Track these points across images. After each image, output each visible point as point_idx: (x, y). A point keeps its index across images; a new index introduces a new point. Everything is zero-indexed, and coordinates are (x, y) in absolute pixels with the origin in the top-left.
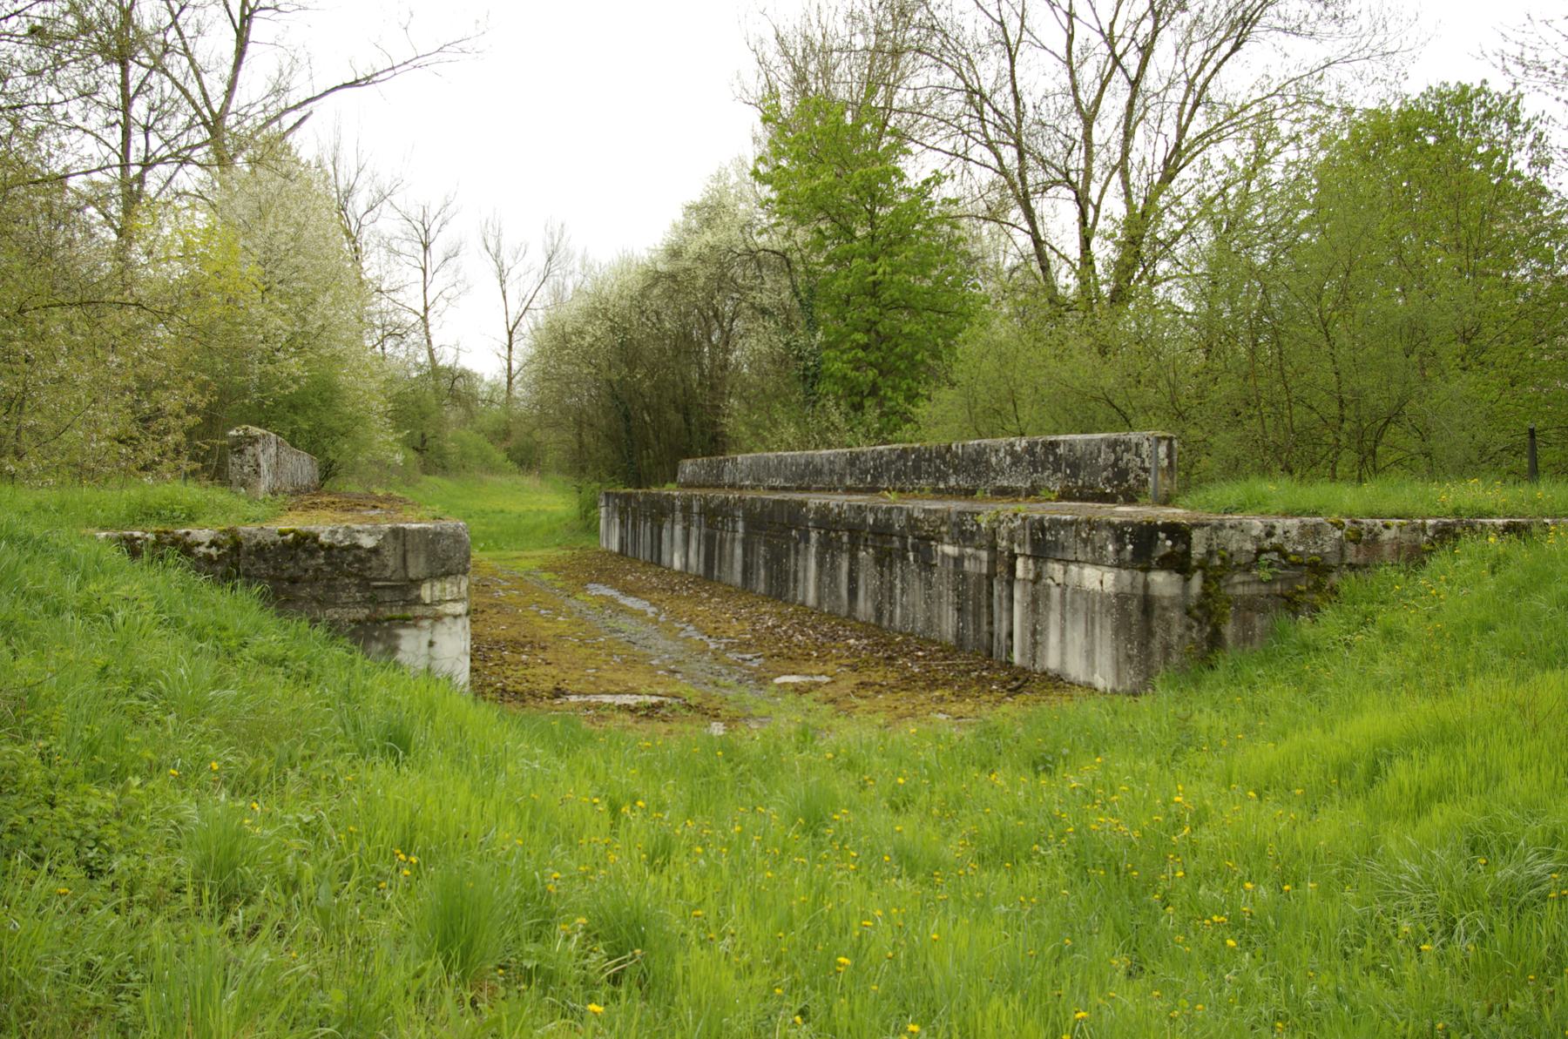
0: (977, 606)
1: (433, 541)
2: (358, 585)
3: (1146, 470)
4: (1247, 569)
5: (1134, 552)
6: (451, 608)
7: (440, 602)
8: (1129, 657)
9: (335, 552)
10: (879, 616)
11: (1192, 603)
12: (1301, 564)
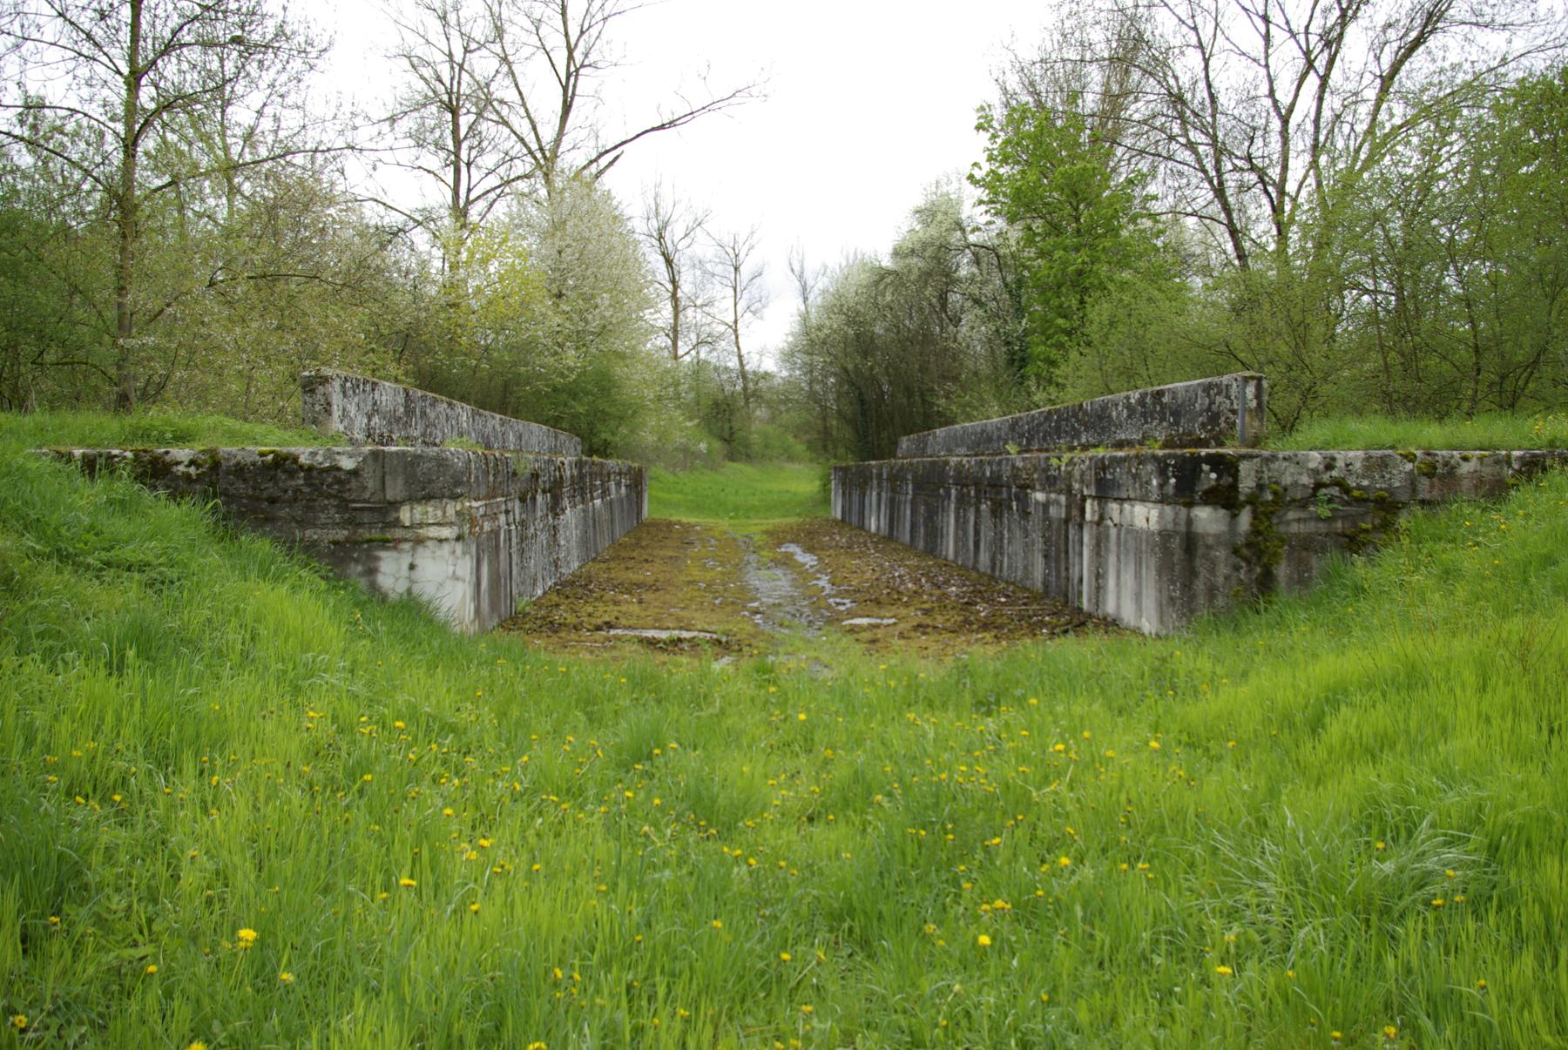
0: (1058, 555)
1: (412, 464)
2: (337, 506)
3: (1234, 412)
4: (1303, 504)
5: (1177, 486)
6: (433, 532)
7: (421, 525)
8: (1172, 599)
9: (315, 473)
10: (993, 569)
11: (1240, 541)
12: (1366, 500)
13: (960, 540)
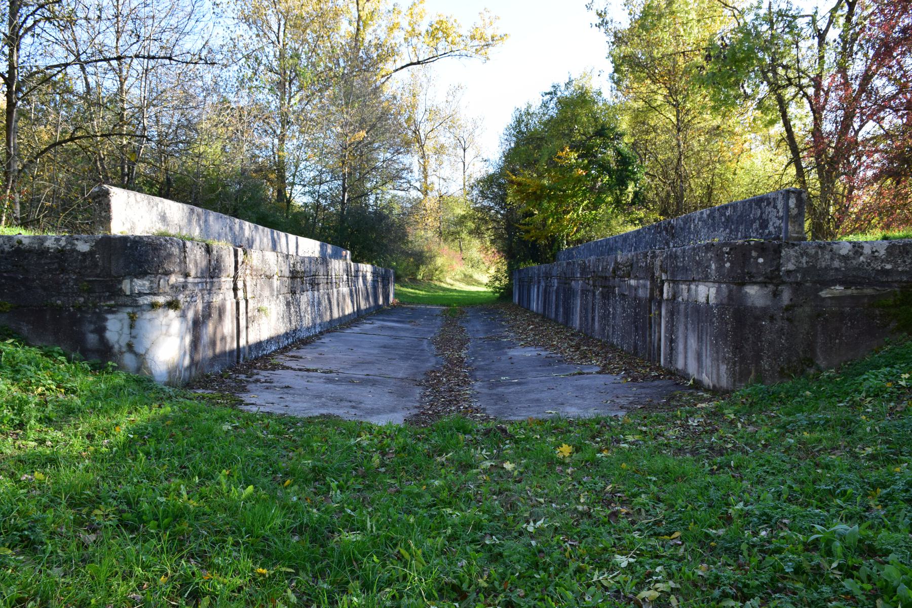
13: (584, 318)
